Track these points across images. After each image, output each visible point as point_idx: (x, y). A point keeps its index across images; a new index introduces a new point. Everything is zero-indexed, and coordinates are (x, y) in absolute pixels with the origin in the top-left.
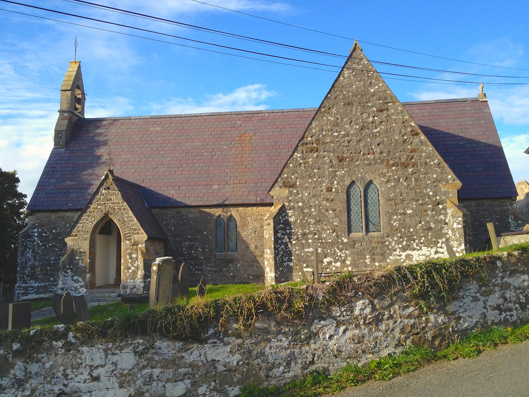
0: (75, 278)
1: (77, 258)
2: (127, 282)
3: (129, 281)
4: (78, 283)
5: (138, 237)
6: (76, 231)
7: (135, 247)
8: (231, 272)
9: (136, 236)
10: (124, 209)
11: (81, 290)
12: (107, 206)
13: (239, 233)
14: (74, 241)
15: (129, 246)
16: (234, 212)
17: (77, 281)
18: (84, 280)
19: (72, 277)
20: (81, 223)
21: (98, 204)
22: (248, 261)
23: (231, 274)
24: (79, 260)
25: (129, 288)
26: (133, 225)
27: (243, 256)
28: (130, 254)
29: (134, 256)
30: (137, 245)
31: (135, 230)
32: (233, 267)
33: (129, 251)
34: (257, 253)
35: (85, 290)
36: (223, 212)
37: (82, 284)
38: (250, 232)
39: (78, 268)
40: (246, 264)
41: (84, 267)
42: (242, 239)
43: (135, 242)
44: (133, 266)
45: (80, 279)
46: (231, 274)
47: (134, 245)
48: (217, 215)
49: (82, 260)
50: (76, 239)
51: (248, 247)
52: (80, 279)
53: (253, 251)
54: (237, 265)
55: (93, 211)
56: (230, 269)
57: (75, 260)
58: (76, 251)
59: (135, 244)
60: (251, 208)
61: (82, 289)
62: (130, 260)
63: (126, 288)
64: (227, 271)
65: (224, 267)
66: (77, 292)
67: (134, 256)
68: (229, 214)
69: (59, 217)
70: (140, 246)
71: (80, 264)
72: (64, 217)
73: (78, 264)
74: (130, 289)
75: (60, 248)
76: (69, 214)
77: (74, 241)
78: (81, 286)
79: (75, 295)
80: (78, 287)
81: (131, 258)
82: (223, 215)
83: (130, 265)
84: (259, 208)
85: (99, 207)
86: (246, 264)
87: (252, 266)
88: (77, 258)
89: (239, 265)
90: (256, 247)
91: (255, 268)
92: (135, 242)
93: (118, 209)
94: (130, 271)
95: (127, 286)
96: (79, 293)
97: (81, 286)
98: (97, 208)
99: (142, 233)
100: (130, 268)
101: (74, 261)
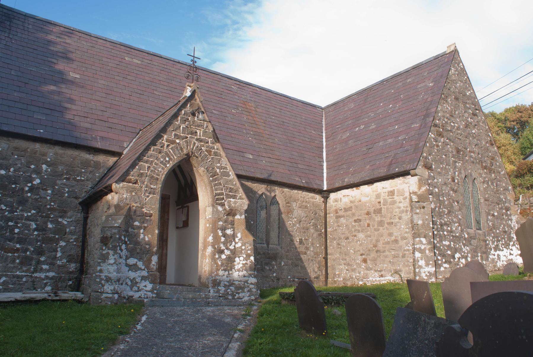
0: (132, 261)
1: (137, 223)
2: (217, 275)
3: (221, 273)
4: (136, 271)
5: (235, 203)
6: (136, 174)
7: (230, 218)
8: (274, 272)
9: (232, 199)
10: (216, 154)
11: (142, 285)
12: (191, 142)
13: (283, 221)
14: (131, 192)
15: (222, 216)
16: (279, 193)
17: (134, 268)
18: (148, 267)
19: (127, 258)
20: (147, 162)
21: (175, 135)
22: (292, 259)
23: (275, 275)
24: (139, 228)
25: (222, 284)
26: (227, 182)
27: (288, 251)
28: (223, 229)
29: (229, 232)
30: (234, 215)
31: (231, 190)
32: (276, 265)
33: (221, 223)
34: (301, 249)
35: (150, 286)
36: (267, 190)
37: (145, 273)
38: (295, 222)
39: (137, 243)
40: (290, 262)
41: (149, 243)
42: (287, 229)
43: (231, 210)
44: (227, 249)
45: (140, 264)
46: (275, 275)
47: (228, 215)
48: (260, 192)
49: (145, 228)
50: (135, 189)
51: (292, 241)
52: (140, 264)
53: (297, 246)
54: (280, 263)
55: (168, 146)
56: (273, 268)
57: (133, 227)
58: (135, 211)
59: (231, 213)
60: (296, 191)
61: (144, 283)
62: (223, 239)
63: (219, 284)
64: (270, 270)
65: (267, 264)
66: (135, 288)
67: (229, 232)
68: (273, 194)
69: (16, 148)
70: (238, 217)
71: (142, 236)
72: (25, 150)
73: (138, 234)
74: (225, 286)
75: (12, 207)
76: (38, 146)
77: (131, 192)
78: (144, 278)
79: (131, 293)
80: (138, 280)
81: (225, 235)
82: (266, 195)
83: (223, 247)
84: (304, 193)
85: (178, 141)
86: (290, 262)
87: (296, 266)
88: (137, 223)
89: (283, 263)
90: (301, 242)
91: (300, 268)
92: (231, 210)
93: (206, 151)
94: (223, 257)
95: (220, 281)
96: (139, 290)
97: (144, 278)
98: (173, 142)
99: (241, 198)
100: (222, 252)
101: (130, 230)
